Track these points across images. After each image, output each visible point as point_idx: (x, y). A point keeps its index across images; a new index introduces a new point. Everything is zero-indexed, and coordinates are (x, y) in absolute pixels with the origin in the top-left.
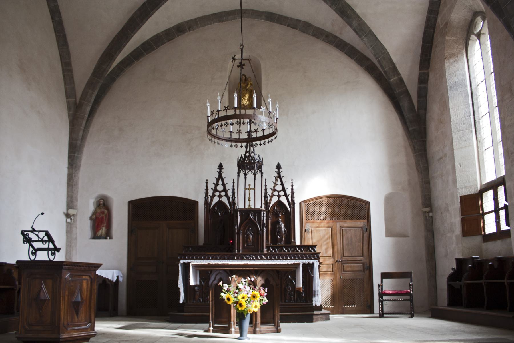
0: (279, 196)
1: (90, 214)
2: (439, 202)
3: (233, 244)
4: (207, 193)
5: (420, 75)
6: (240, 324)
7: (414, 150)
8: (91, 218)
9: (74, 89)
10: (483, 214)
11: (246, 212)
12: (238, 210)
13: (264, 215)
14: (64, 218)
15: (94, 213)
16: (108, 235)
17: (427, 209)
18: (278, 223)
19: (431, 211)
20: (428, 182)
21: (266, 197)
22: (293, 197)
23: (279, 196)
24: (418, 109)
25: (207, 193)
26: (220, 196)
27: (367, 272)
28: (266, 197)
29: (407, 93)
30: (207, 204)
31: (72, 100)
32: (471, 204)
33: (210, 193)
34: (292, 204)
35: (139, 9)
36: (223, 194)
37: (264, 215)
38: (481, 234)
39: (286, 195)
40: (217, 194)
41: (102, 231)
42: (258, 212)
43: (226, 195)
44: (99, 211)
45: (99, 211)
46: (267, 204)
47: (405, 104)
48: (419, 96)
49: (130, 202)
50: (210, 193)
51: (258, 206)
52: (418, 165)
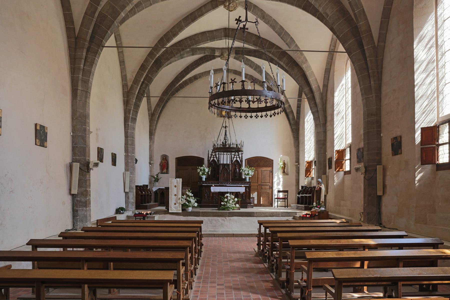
0: (237, 158)
1: (159, 163)
2: (301, 162)
3: (219, 177)
4: (208, 156)
5: (298, 104)
6: (198, 283)
7: (294, 137)
8: (160, 165)
9: (151, 107)
10: (439, 145)
11: (224, 165)
12: (221, 164)
13: (231, 166)
14: (149, 164)
15: (161, 162)
16: (167, 173)
17: (297, 164)
18: (236, 169)
19: (299, 164)
20: (299, 152)
21: (231, 158)
22: (242, 159)
23: (237, 158)
24: (379, 42)
25: (208, 156)
26: (214, 157)
27: (271, 190)
28: (231, 158)
29: (292, 112)
30: (209, 161)
31: (150, 112)
32: (430, 134)
33: (210, 156)
34: (242, 161)
35: (180, 73)
36: (215, 156)
37: (231, 166)
38: (435, 163)
39: (239, 157)
40: (212, 156)
41: (165, 171)
42: (228, 165)
43: (216, 157)
44: (163, 162)
45: (163, 162)
46: (232, 161)
47: (291, 117)
48: (297, 113)
49: (176, 158)
50: (210, 156)
51: (228, 163)
52: (294, 144)
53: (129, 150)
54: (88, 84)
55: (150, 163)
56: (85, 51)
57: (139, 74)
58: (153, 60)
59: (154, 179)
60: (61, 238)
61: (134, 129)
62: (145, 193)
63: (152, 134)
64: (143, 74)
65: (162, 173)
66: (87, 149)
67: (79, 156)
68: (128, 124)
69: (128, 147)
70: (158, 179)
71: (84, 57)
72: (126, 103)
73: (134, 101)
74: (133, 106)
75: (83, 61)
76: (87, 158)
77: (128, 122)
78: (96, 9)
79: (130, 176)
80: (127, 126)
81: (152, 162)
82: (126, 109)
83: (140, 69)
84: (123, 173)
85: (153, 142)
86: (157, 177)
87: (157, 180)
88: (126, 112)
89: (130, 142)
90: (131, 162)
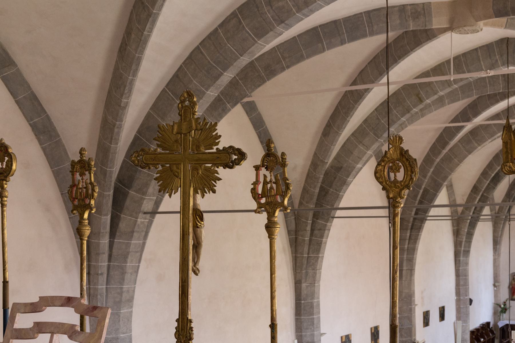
1: (507, 285)
53: (461, 293)
54: (412, 262)
55: (494, 286)
56: (409, 231)
57: (471, 198)
58: (487, 180)
59: (500, 309)
60: (217, 141)
61: (467, 264)
62: (484, 338)
63: (496, 243)
64: (476, 198)
65: (512, 300)
66: (413, 328)
67: (405, 337)
68: (460, 260)
69: (459, 289)
70: (506, 309)
71: (408, 238)
72: (457, 233)
73: (466, 230)
74: (464, 237)
75: (407, 241)
76: (413, 338)
77: (459, 257)
78: (419, 192)
79: (463, 326)
80: (457, 262)
81: (497, 284)
82: (456, 240)
83: (472, 191)
84: (454, 323)
85: (499, 255)
86: (505, 305)
87: (504, 310)
88: (457, 244)
89: (462, 283)
90: (464, 301)
